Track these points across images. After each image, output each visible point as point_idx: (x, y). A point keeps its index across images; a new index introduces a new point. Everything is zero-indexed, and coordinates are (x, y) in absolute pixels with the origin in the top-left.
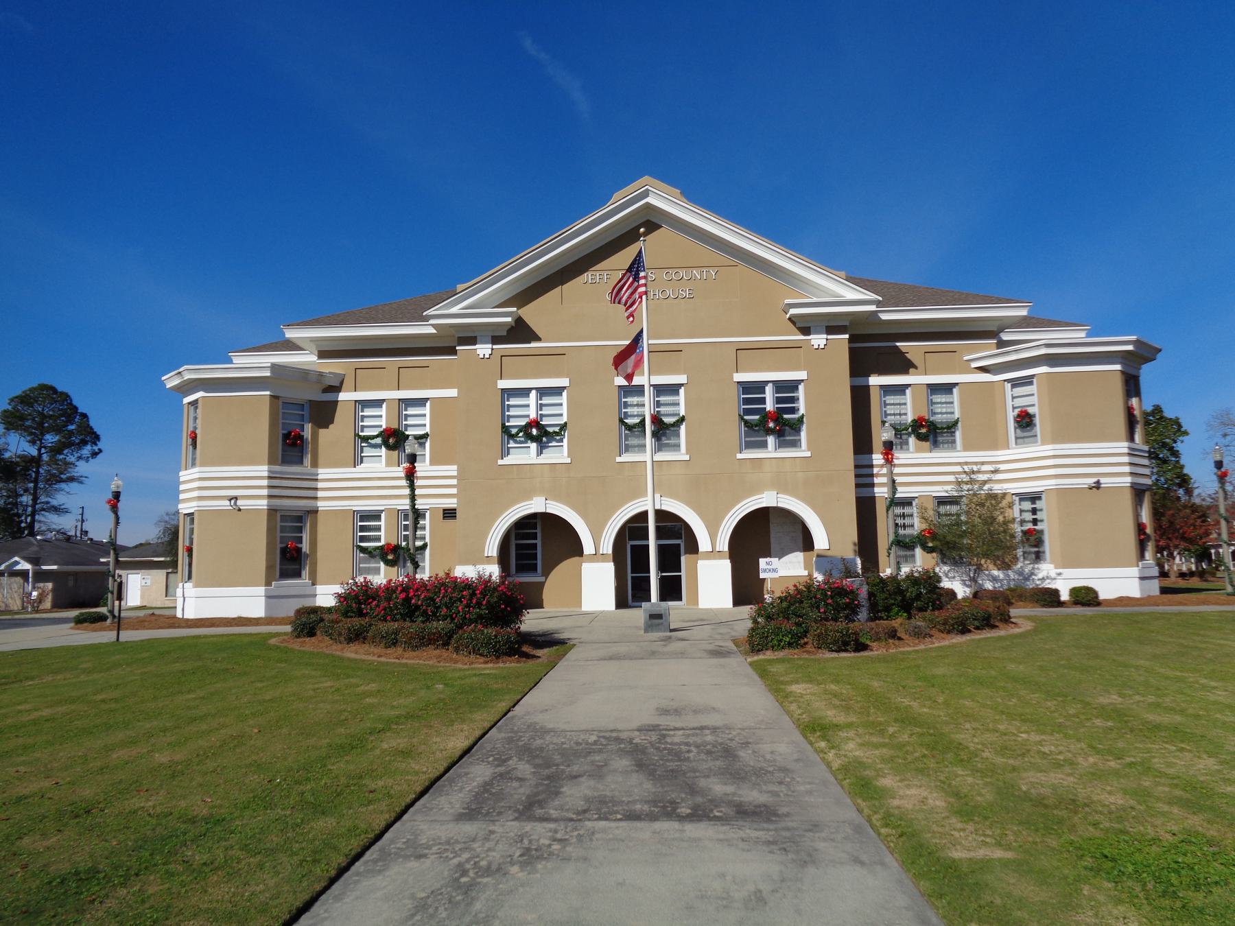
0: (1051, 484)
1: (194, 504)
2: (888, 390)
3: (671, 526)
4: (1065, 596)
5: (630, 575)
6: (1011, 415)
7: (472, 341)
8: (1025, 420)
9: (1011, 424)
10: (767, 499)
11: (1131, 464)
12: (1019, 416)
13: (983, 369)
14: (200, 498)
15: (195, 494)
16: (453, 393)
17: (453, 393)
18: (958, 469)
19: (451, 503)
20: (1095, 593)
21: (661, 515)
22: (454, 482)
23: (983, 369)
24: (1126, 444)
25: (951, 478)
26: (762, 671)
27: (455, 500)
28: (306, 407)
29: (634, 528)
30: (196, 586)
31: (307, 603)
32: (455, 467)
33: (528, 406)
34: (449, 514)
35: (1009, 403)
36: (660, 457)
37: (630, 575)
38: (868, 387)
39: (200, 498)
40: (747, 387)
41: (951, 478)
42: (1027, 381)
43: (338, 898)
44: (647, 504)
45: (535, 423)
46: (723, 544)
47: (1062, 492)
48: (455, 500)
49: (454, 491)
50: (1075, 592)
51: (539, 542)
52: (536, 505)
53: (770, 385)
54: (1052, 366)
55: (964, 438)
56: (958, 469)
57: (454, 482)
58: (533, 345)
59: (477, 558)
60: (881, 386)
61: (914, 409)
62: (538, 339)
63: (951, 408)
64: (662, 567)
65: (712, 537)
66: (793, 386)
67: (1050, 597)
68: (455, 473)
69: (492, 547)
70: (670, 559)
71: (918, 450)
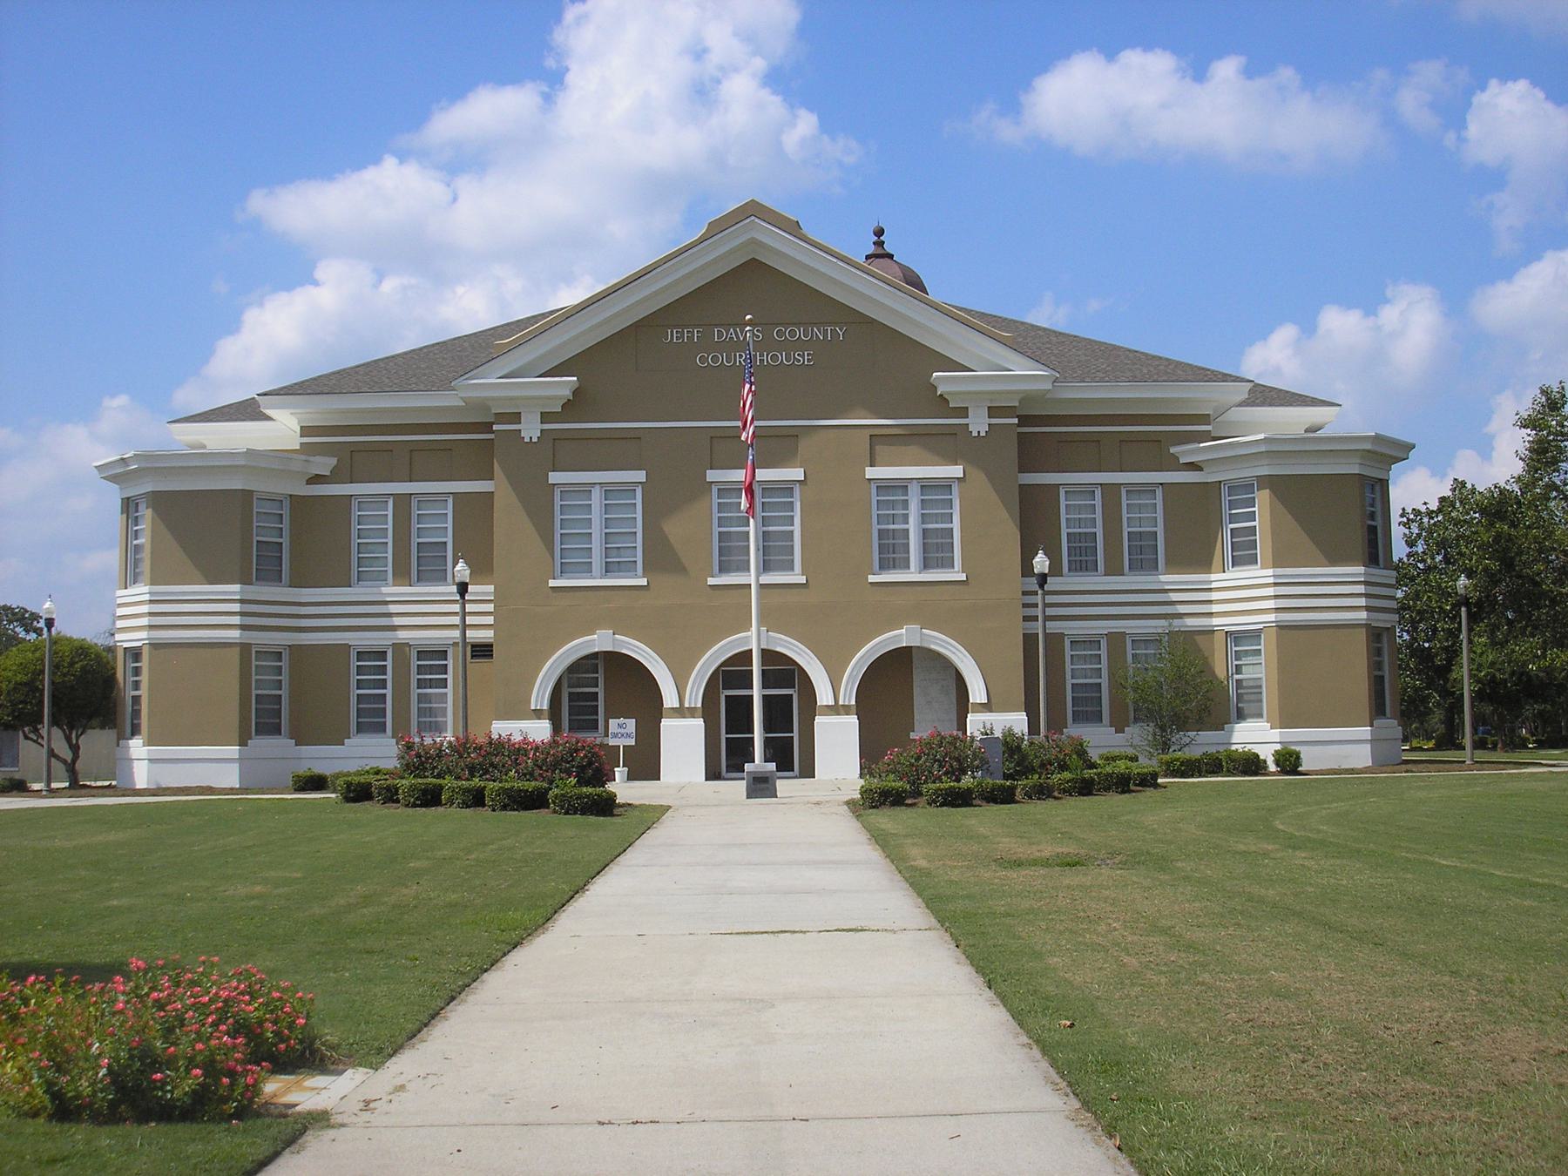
3: (782, 671)
5: (724, 736)
10: (903, 636)
11: (1366, 595)
14: (151, 627)
21: (769, 656)
22: (490, 607)
26: (880, 839)
28: (286, 504)
29: (733, 673)
30: (149, 743)
32: (491, 588)
36: (767, 579)
37: (724, 736)
43: (446, 1018)
44: (753, 639)
46: (849, 697)
47: (155, 646)
49: (490, 620)
51: (600, 690)
52: (601, 640)
57: (490, 607)
59: (519, 710)
64: (768, 726)
65: (832, 687)
67: (1252, 765)
69: (540, 697)
70: (778, 713)
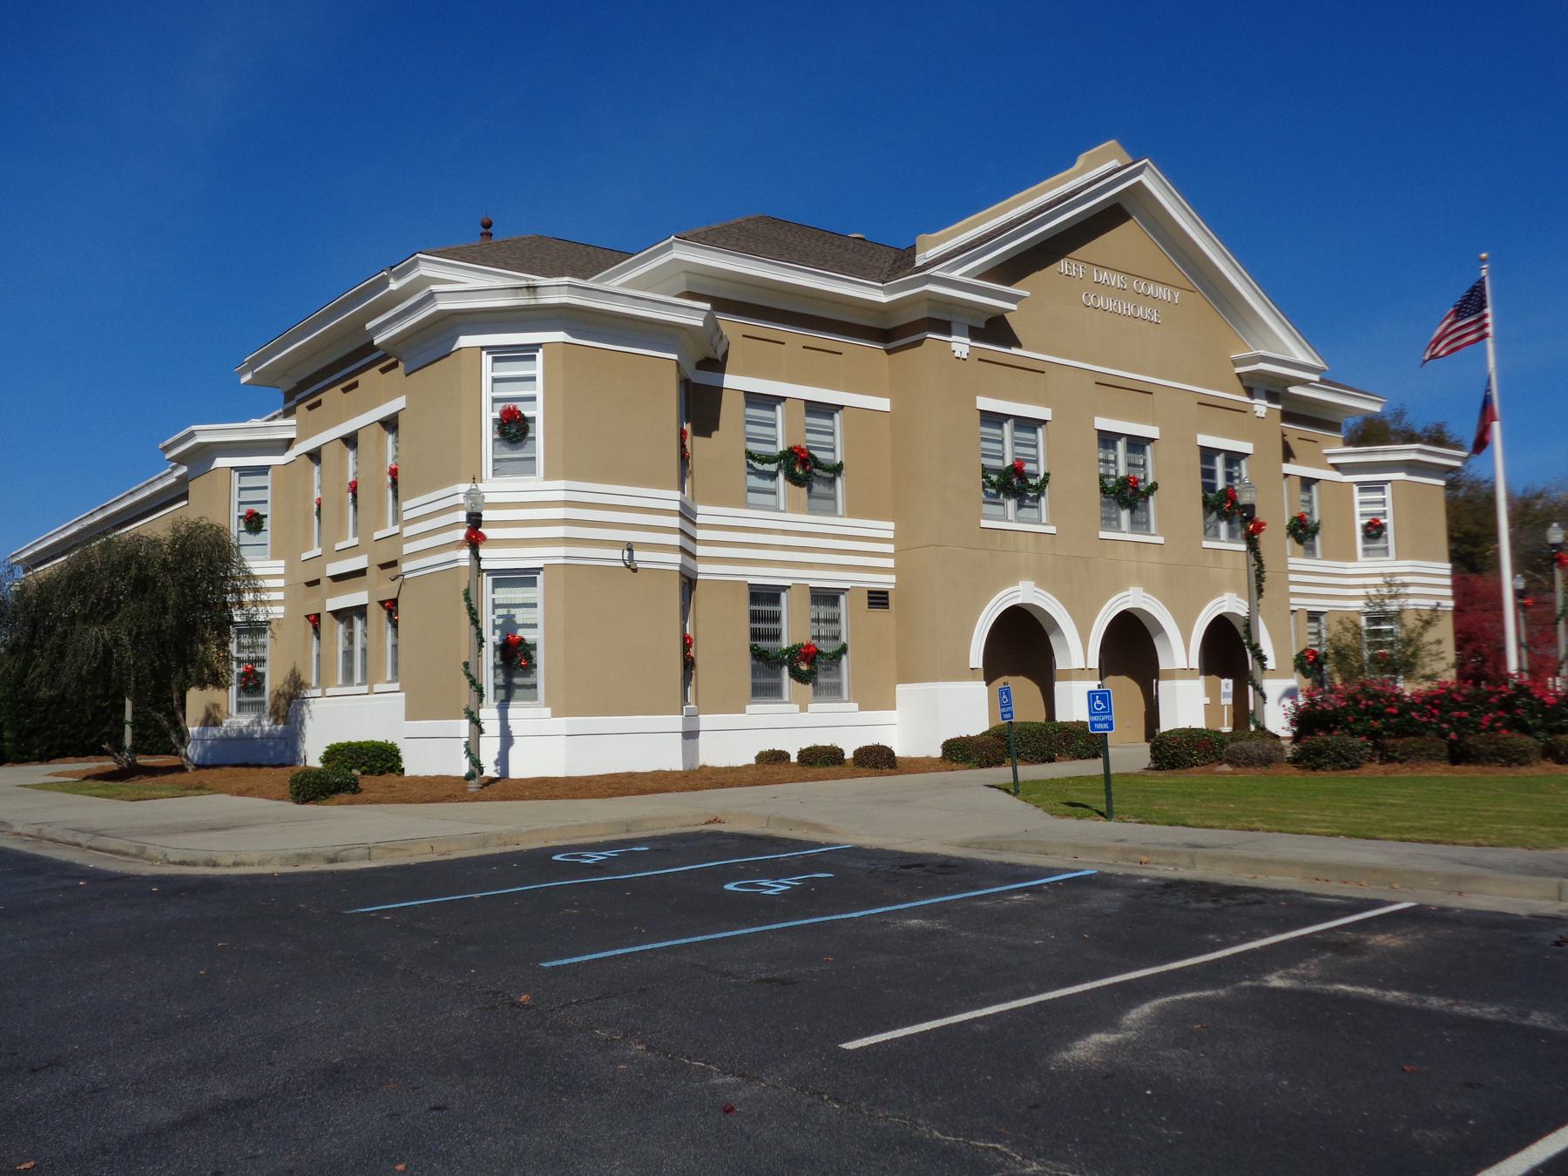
0: (557, 554)
1: (561, 551)
2: (753, 399)
4: (849, 755)
6: (490, 415)
7: (945, 328)
8: (513, 428)
9: (1359, 534)
12: (1369, 524)
13: (1336, 467)
15: (559, 531)
16: (883, 404)
17: (883, 404)
18: (1379, 580)
19: (886, 582)
20: (890, 753)
23: (1336, 467)
24: (677, 495)
25: (1362, 592)
27: (892, 578)
31: (296, 770)
33: (533, 379)
34: (878, 599)
35: (1358, 509)
38: (718, 391)
39: (568, 541)
40: (1208, 454)
41: (1362, 592)
42: (1378, 487)
45: (1017, 470)
47: (569, 571)
48: (892, 578)
50: (802, 754)
53: (1011, 421)
54: (1410, 474)
55: (1322, 545)
56: (1379, 580)
57: (890, 548)
58: (1014, 351)
60: (1303, 478)
61: (787, 435)
62: (1019, 345)
63: (834, 445)
66: (1233, 458)
68: (891, 535)
71: (793, 507)
